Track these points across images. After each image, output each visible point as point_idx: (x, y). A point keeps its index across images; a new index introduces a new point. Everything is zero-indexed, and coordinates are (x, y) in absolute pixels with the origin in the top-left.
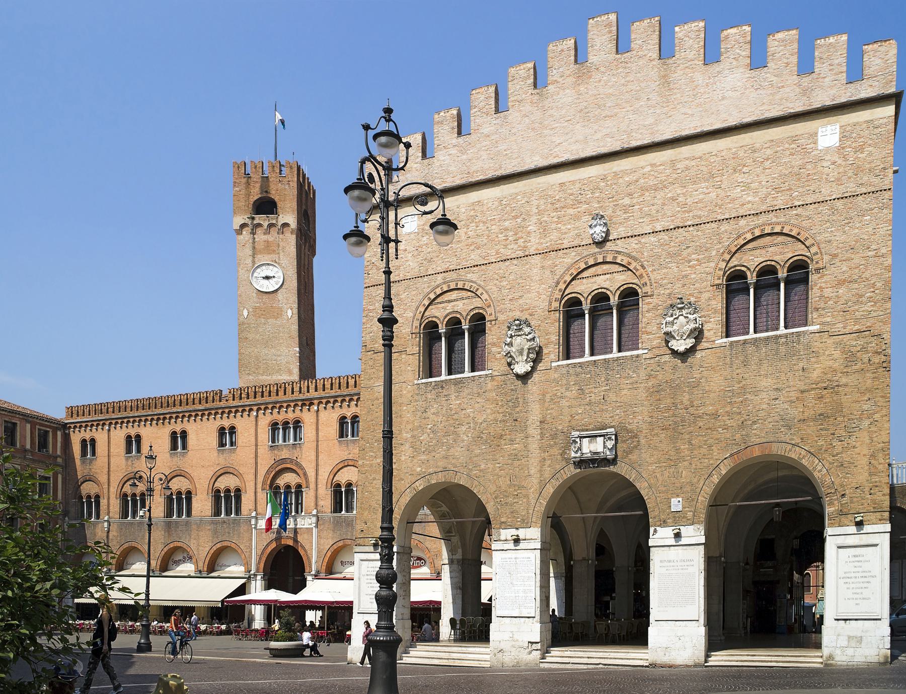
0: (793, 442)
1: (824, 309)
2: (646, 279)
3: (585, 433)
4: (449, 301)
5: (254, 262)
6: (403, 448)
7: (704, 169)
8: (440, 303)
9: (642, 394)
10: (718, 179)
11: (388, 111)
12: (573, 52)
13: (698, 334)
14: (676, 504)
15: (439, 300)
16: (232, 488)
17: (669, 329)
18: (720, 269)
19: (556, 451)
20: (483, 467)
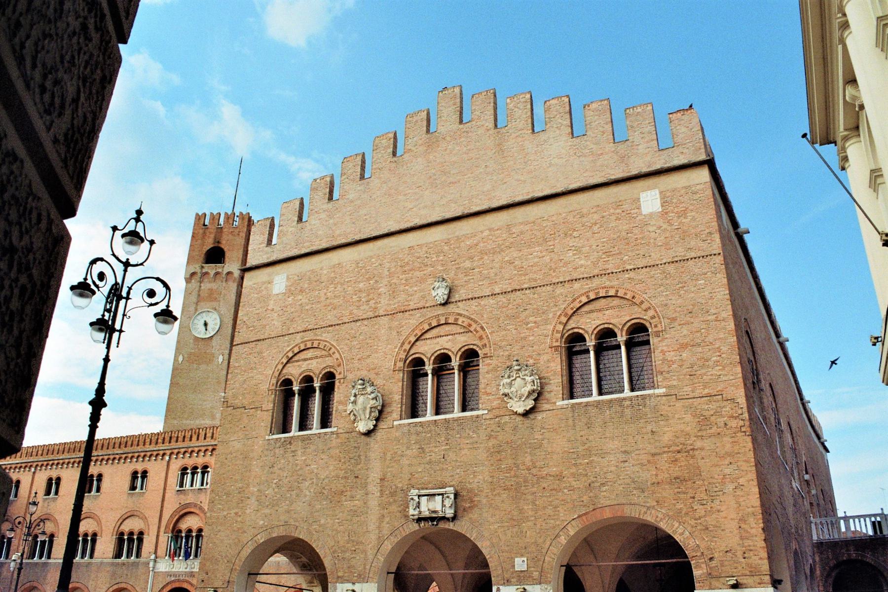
0: (648, 505)
1: (668, 372)
2: (485, 341)
3: (423, 492)
4: (305, 360)
5: (196, 310)
6: (248, 502)
7: (538, 234)
8: (297, 361)
9: (482, 455)
10: (550, 243)
11: (139, 212)
12: (425, 123)
13: (538, 395)
14: (520, 564)
15: (296, 358)
16: (136, 531)
17: (506, 391)
18: (558, 332)
19: (394, 508)
20: (322, 522)
